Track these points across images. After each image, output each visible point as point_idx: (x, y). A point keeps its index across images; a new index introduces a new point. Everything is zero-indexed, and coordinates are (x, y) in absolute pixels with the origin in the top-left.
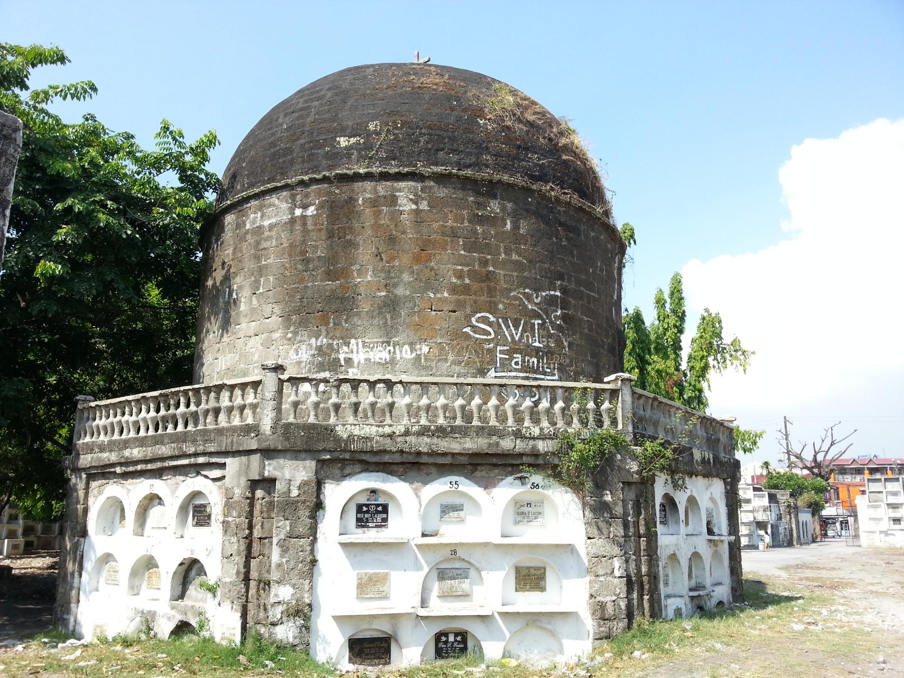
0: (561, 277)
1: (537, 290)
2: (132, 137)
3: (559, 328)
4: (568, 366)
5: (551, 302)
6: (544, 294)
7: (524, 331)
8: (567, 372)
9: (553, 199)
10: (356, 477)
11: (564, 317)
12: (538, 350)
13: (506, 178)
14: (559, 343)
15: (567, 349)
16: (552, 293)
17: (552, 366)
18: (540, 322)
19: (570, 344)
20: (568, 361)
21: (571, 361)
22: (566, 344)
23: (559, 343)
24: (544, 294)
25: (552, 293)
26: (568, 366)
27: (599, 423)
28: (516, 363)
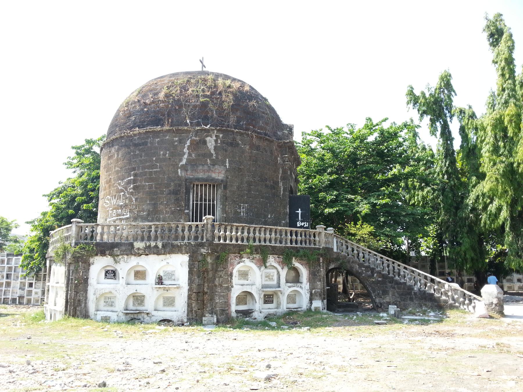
0: (134, 169)
1: (122, 180)
2: (501, 15)
3: (132, 193)
4: (134, 209)
5: (129, 182)
6: (125, 180)
7: (117, 199)
8: (133, 212)
9: (133, 135)
10: (88, 309)
11: (134, 188)
12: (121, 206)
13: (215, 112)
14: (130, 200)
15: (134, 202)
16: (129, 178)
17: (127, 211)
18: (123, 193)
19: (136, 199)
20: (134, 207)
21: (136, 206)
22: (134, 199)
23: (130, 200)
24: (125, 180)
25: (129, 178)
26: (134, 209)
27: (260, 241)
28: (114, 214)
